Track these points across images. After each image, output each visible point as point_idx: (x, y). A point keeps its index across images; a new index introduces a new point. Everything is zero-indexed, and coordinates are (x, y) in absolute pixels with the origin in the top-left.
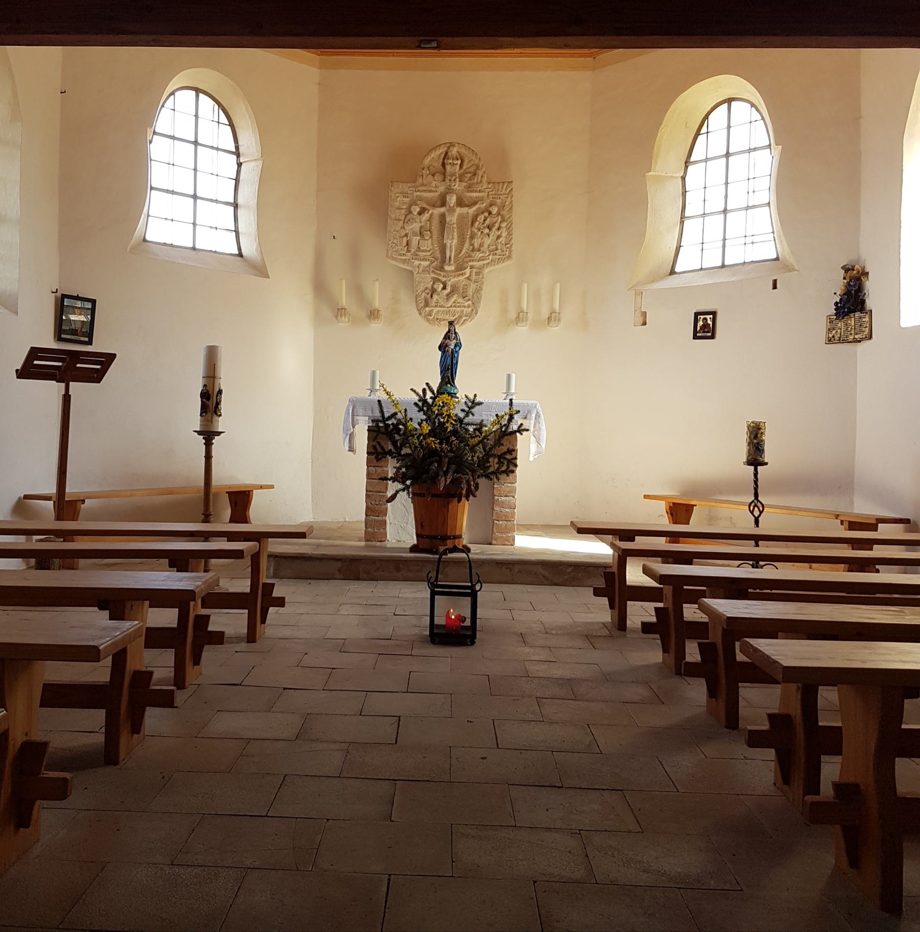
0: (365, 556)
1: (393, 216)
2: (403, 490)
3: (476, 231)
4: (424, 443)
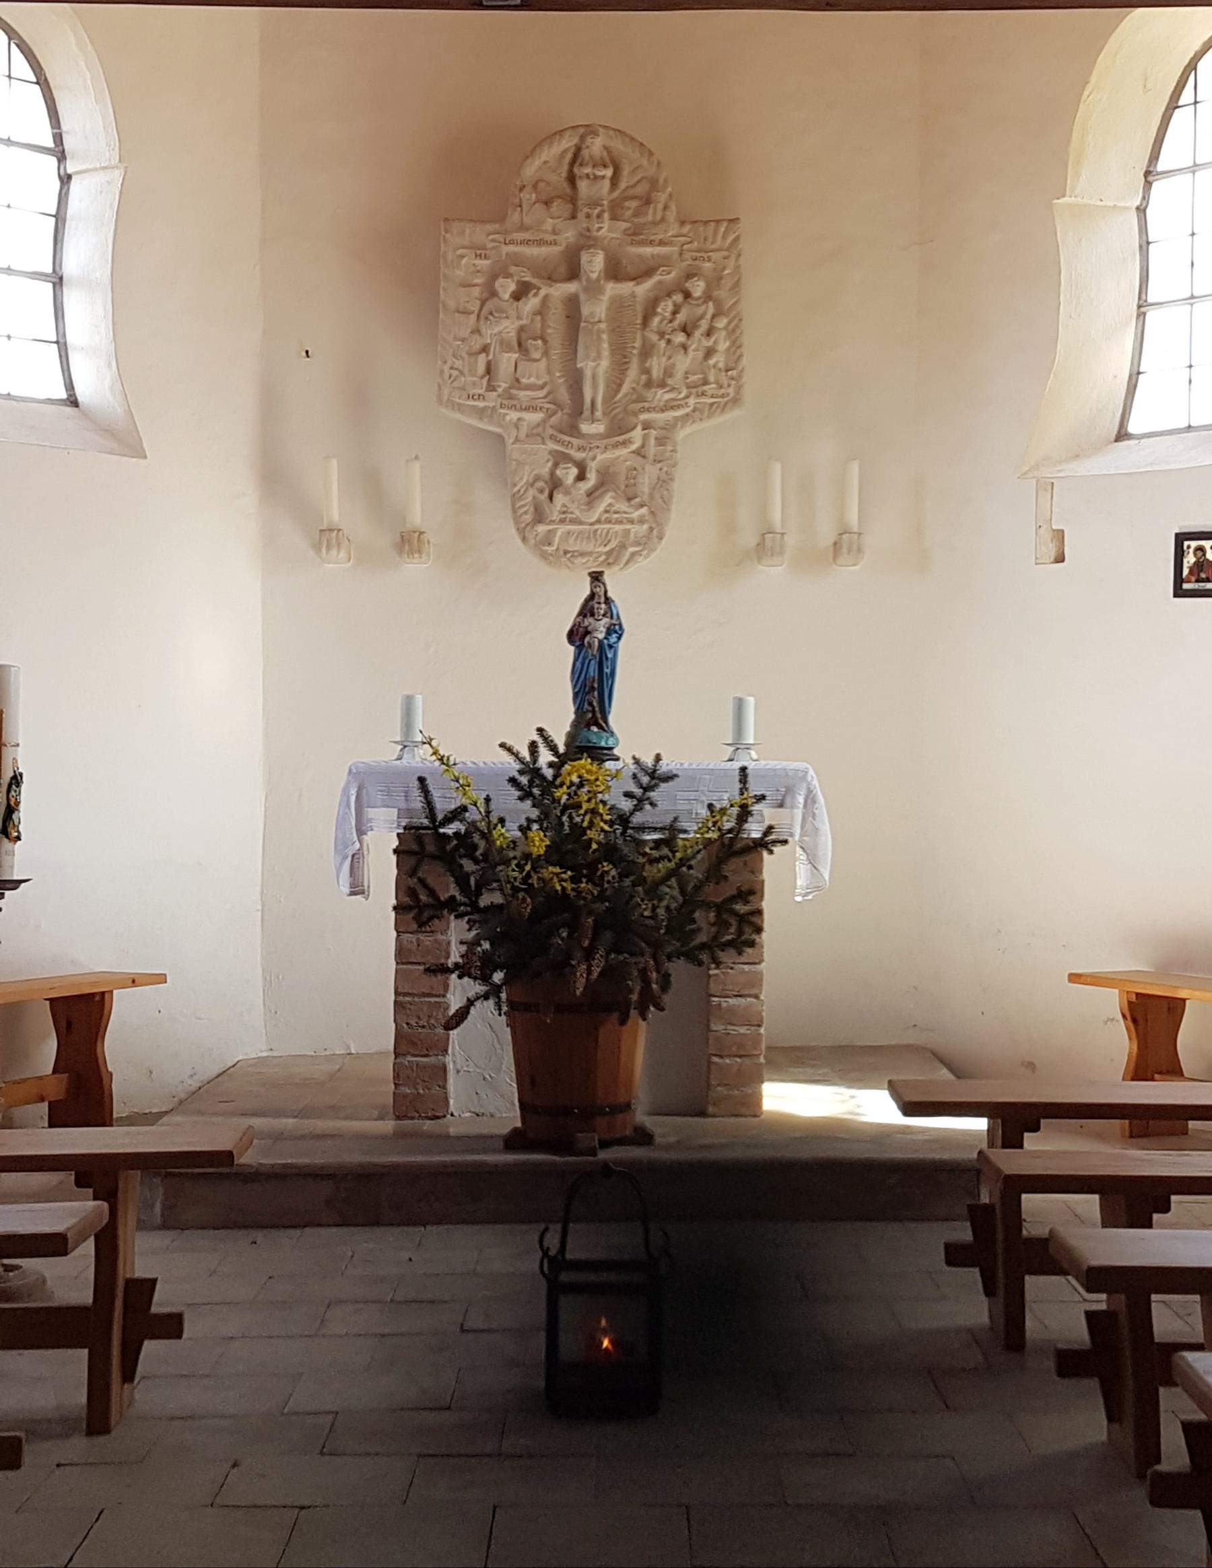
0: (395, 1167)
1: (451, 304)
2: (486, 997)
3: (655, 338)
4: (534, 880)
